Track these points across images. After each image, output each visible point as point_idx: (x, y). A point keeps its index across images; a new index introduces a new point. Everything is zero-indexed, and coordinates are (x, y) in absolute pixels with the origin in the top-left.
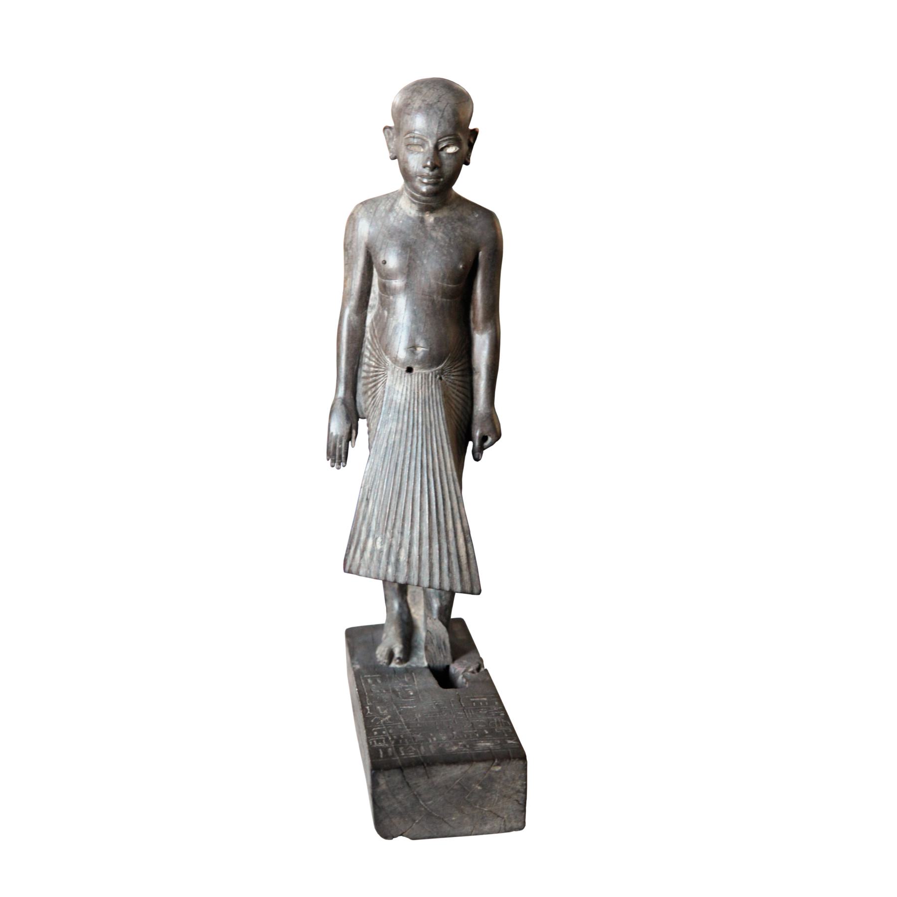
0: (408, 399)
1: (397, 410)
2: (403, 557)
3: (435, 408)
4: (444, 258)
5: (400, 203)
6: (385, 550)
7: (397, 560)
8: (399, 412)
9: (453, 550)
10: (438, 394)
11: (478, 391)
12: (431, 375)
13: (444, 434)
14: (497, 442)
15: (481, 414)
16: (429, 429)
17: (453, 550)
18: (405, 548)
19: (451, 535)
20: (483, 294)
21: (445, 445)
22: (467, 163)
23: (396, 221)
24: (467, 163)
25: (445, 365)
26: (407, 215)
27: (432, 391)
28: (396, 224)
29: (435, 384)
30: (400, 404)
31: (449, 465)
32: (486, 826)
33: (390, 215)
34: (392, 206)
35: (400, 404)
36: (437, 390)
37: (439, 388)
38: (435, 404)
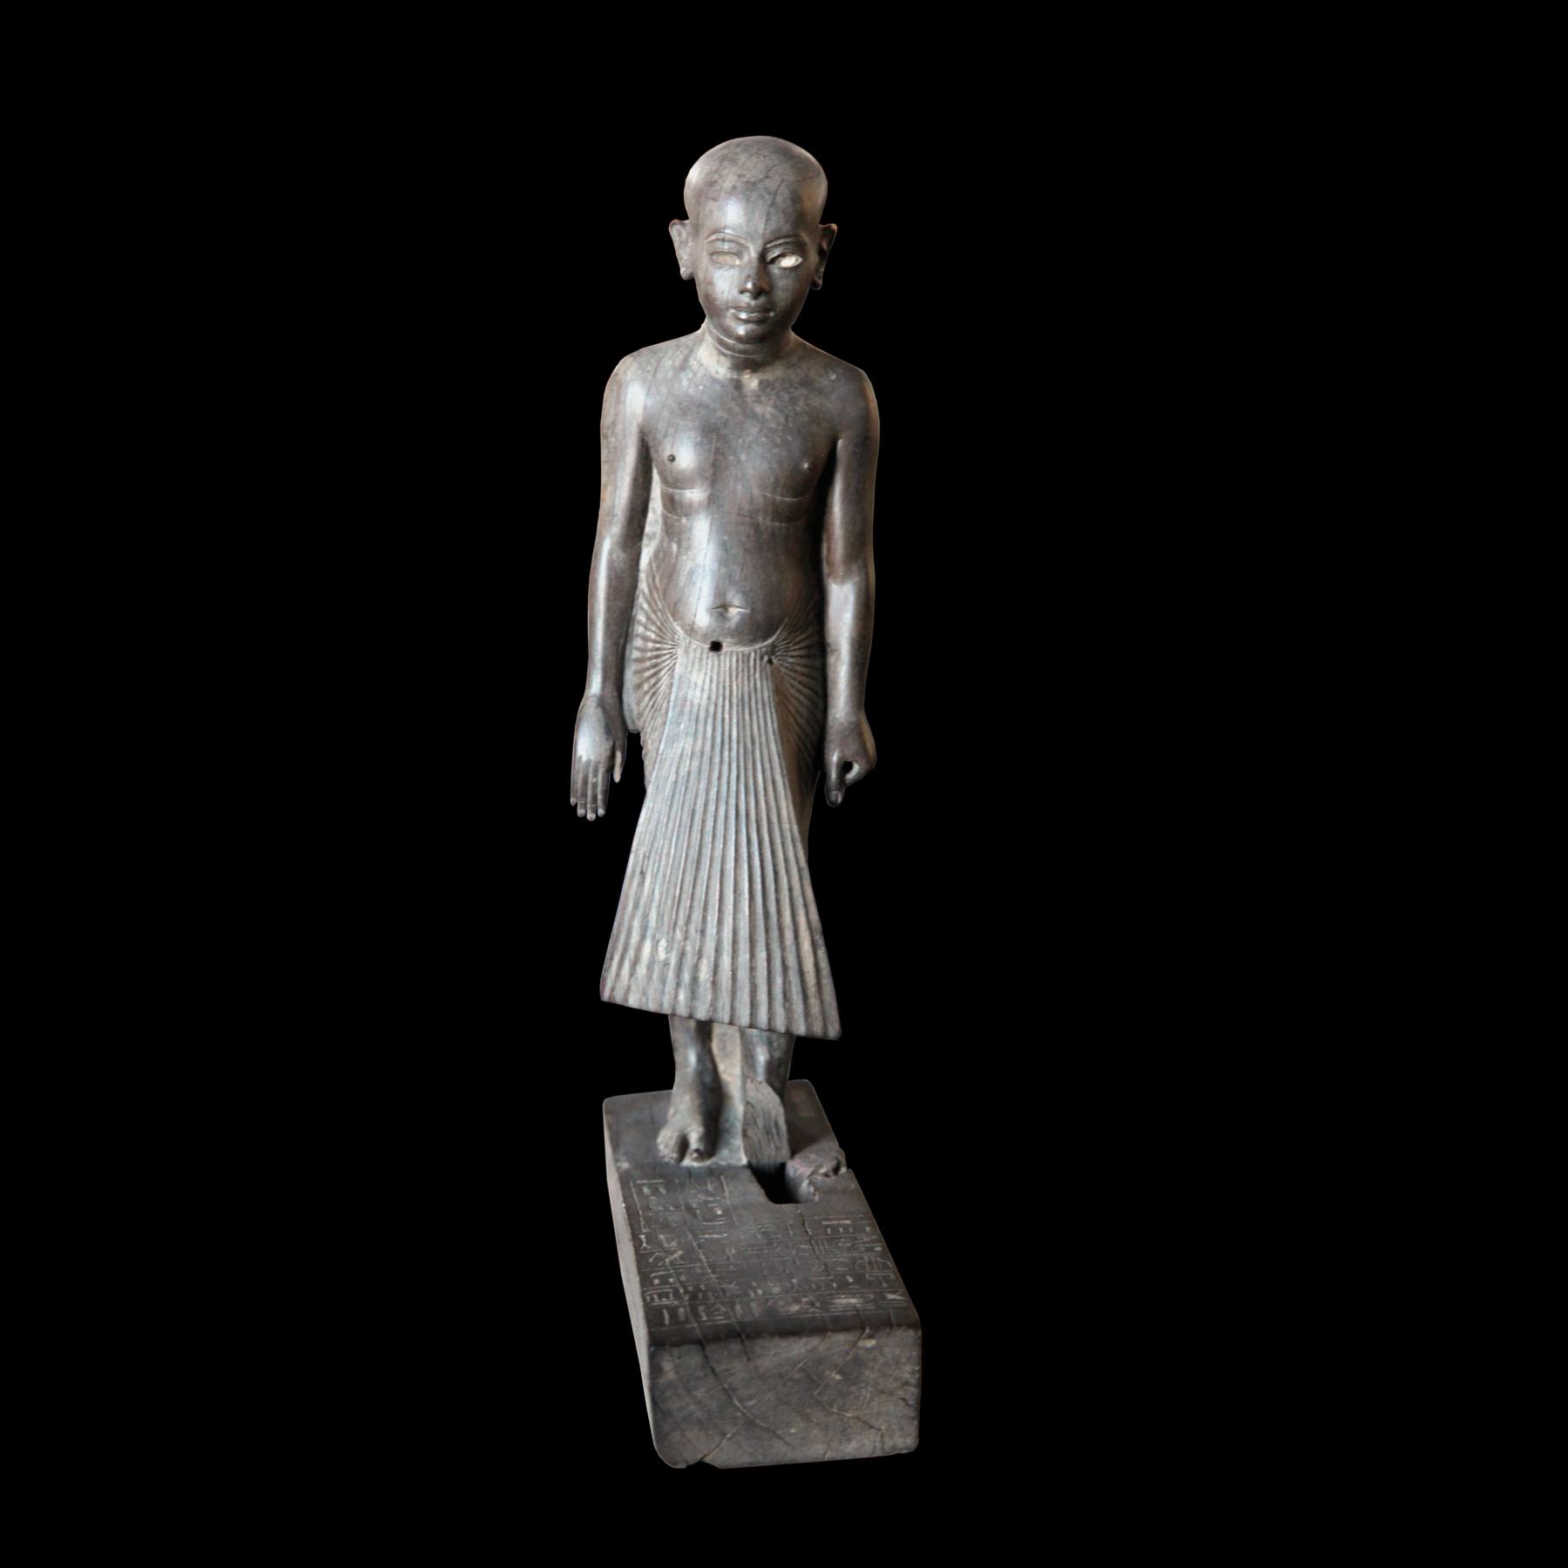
2: (705, 974)
3: (761, 713)
4: (776, 451)
6: (673, 961)
7: (695, 979)
9: (792, 961)
10: (765, 688)
12: (753, 655)
13: (775, 758)
17: (792, 961)
19: (789, 935)
21: (778, 778)
25: (777, 639)
27: (755, 684)
31: (784, 813)
36: (765, 682)
37: (767, 679)
38: (760, 706)
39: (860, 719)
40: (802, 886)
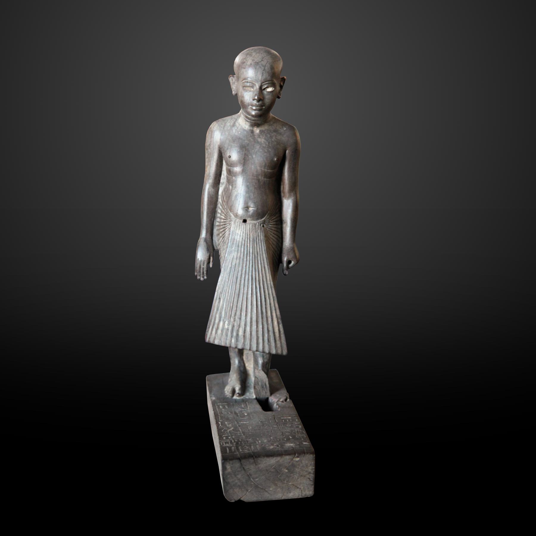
2: (241, 333)
3: (260, 244)
6: (230, 329)
7: (237, 335)
9: (271, 328)
10: (262, 235)
12: (257, 224)
13: (265, 259)
17: (271, 328)
19: (270, 319)
21: (266, 266)
25: (266, 218)
27: (258, 234)
29: (260, 230)
31: (268, 278)
36: (261, 233)
37: (262, 232)
38: (260, 241)
39: (294, 246)
40: (274, 303)
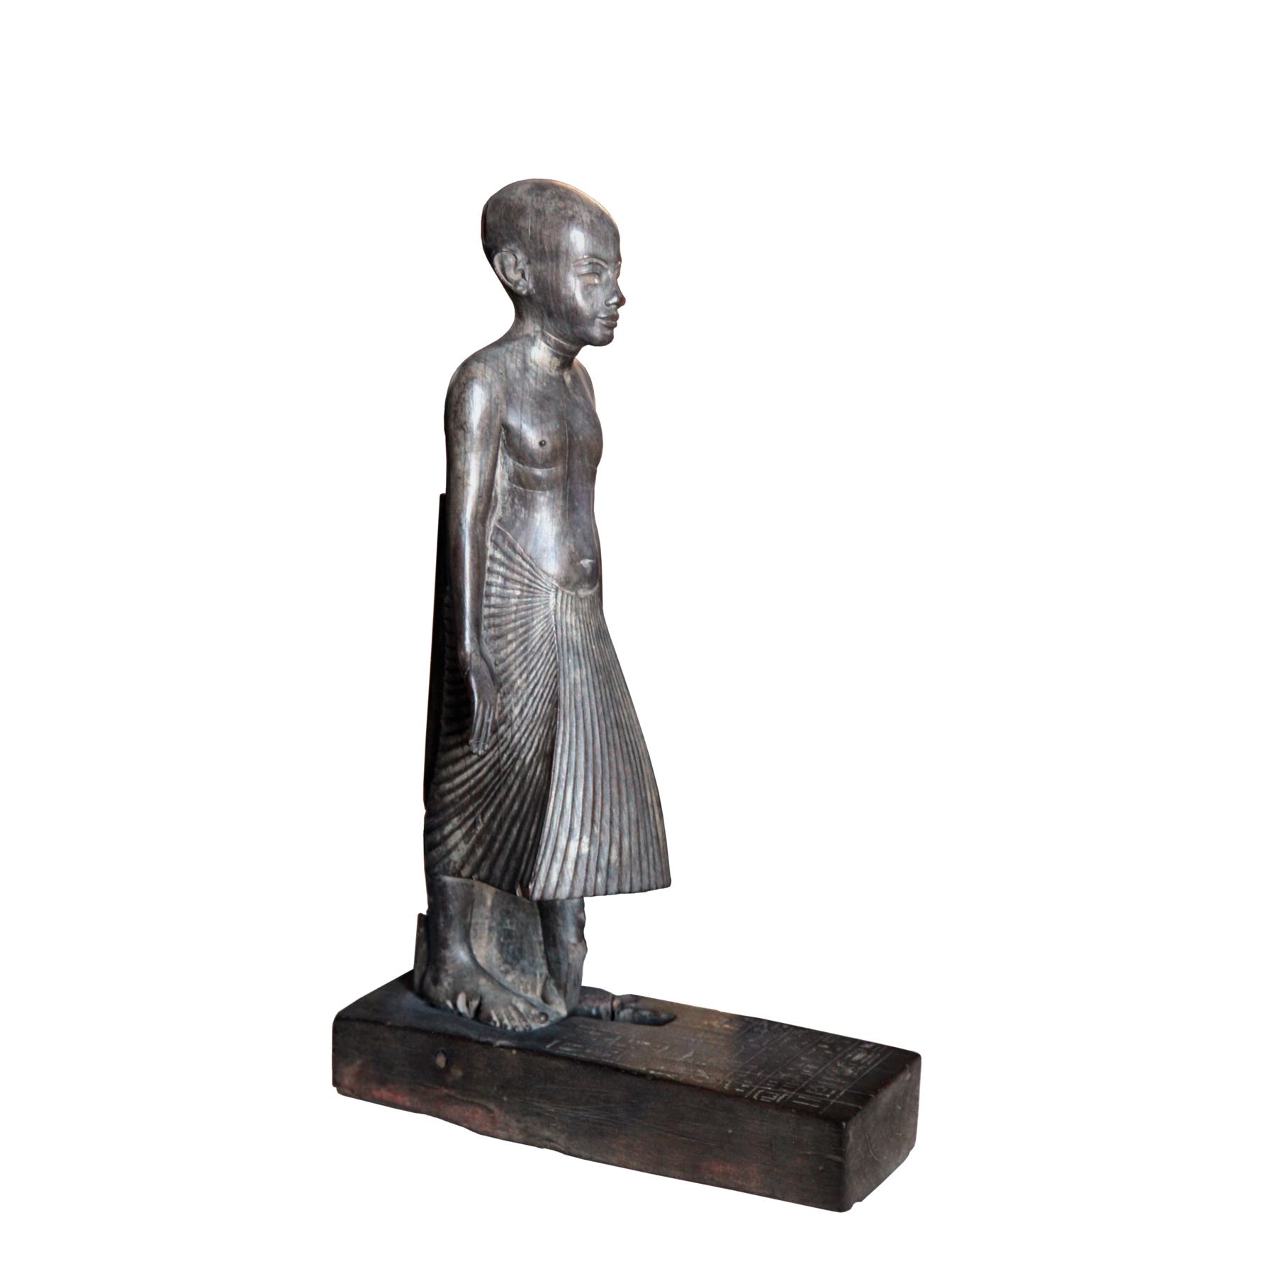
0: (584, 634)
1: (576, 651)
5: (532, 357)
8: (578, 654)
11: (464, 486)
14: (561, 1154)
15: (477, 382)
16: (651, 867)
18: (578, 818)
20: (474, 698)
22: (420, 916)
23: (538, 383)
24: (420, 916)
26: (548, 375)
28: (539, 387)
30: (577, 641)
32: (441, 985)
33: (528, 375)
34: (524, 361)
35: (577, 641)
